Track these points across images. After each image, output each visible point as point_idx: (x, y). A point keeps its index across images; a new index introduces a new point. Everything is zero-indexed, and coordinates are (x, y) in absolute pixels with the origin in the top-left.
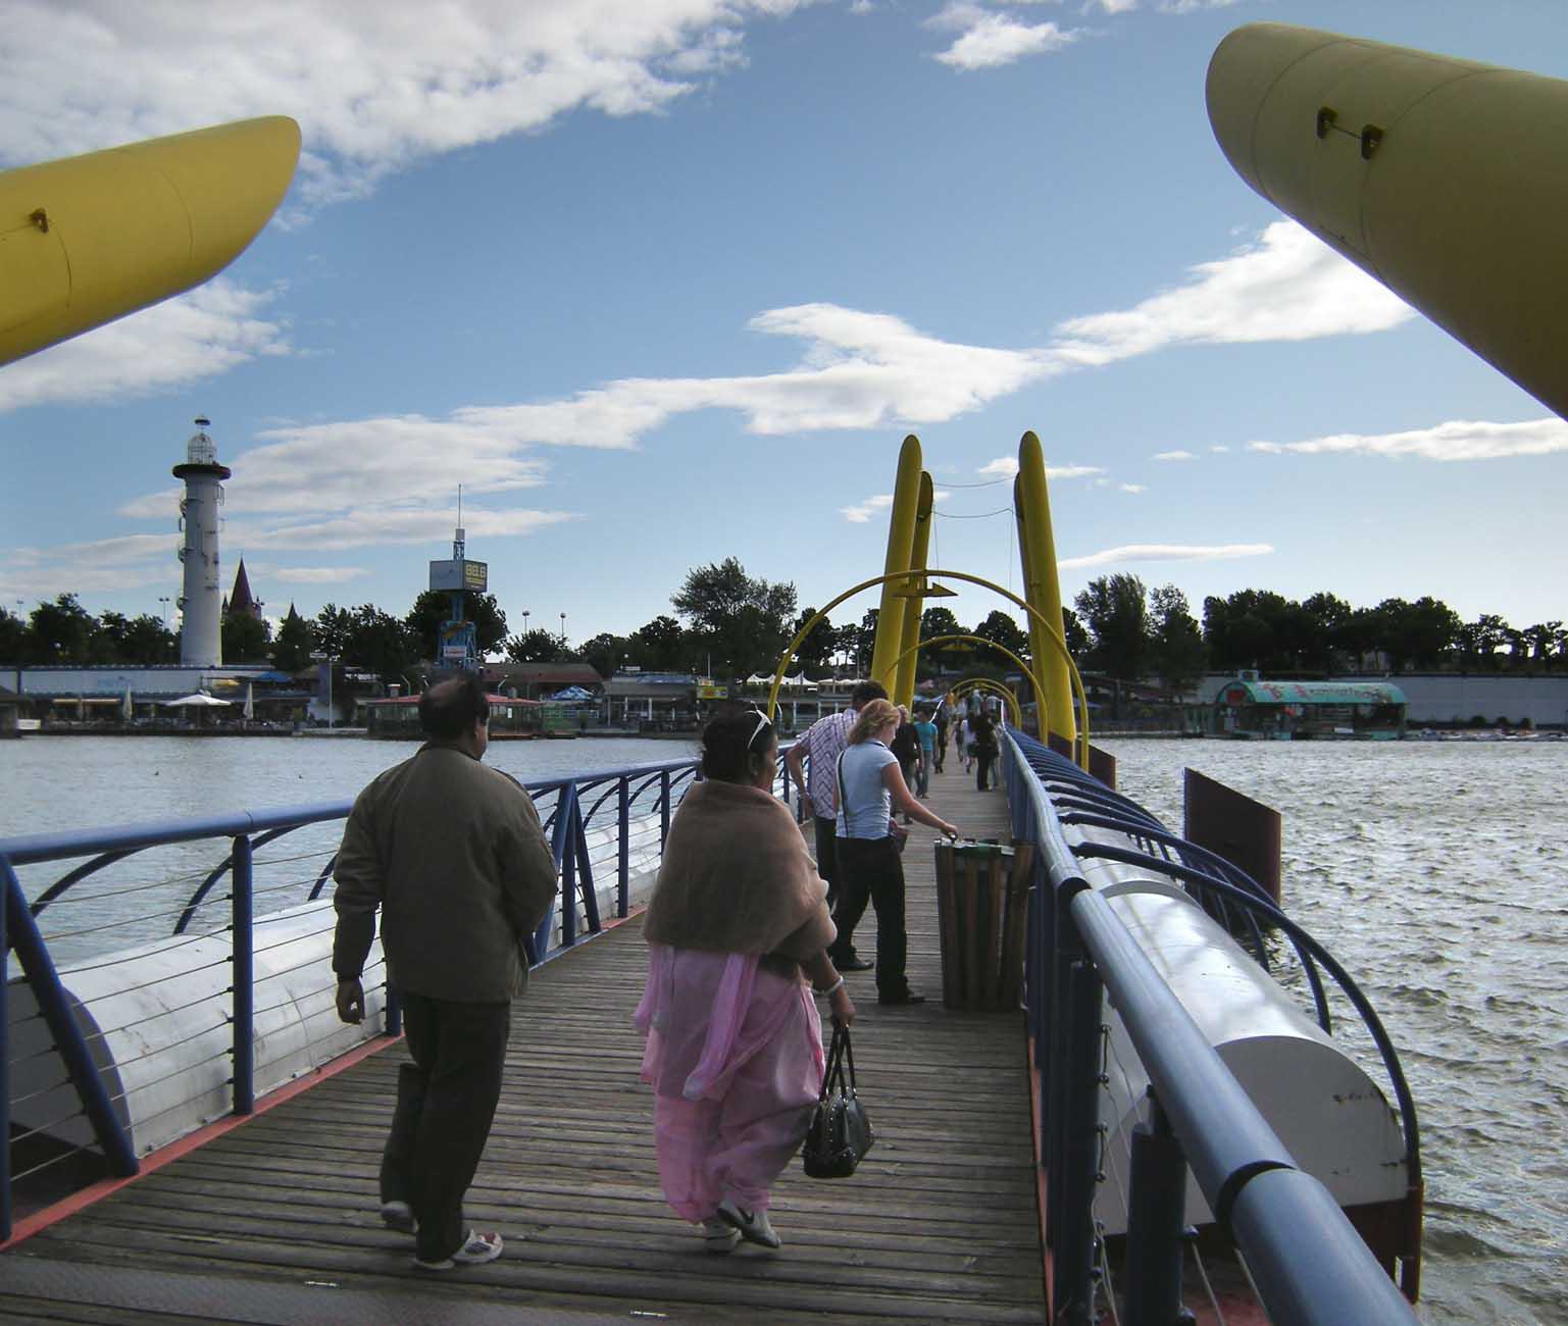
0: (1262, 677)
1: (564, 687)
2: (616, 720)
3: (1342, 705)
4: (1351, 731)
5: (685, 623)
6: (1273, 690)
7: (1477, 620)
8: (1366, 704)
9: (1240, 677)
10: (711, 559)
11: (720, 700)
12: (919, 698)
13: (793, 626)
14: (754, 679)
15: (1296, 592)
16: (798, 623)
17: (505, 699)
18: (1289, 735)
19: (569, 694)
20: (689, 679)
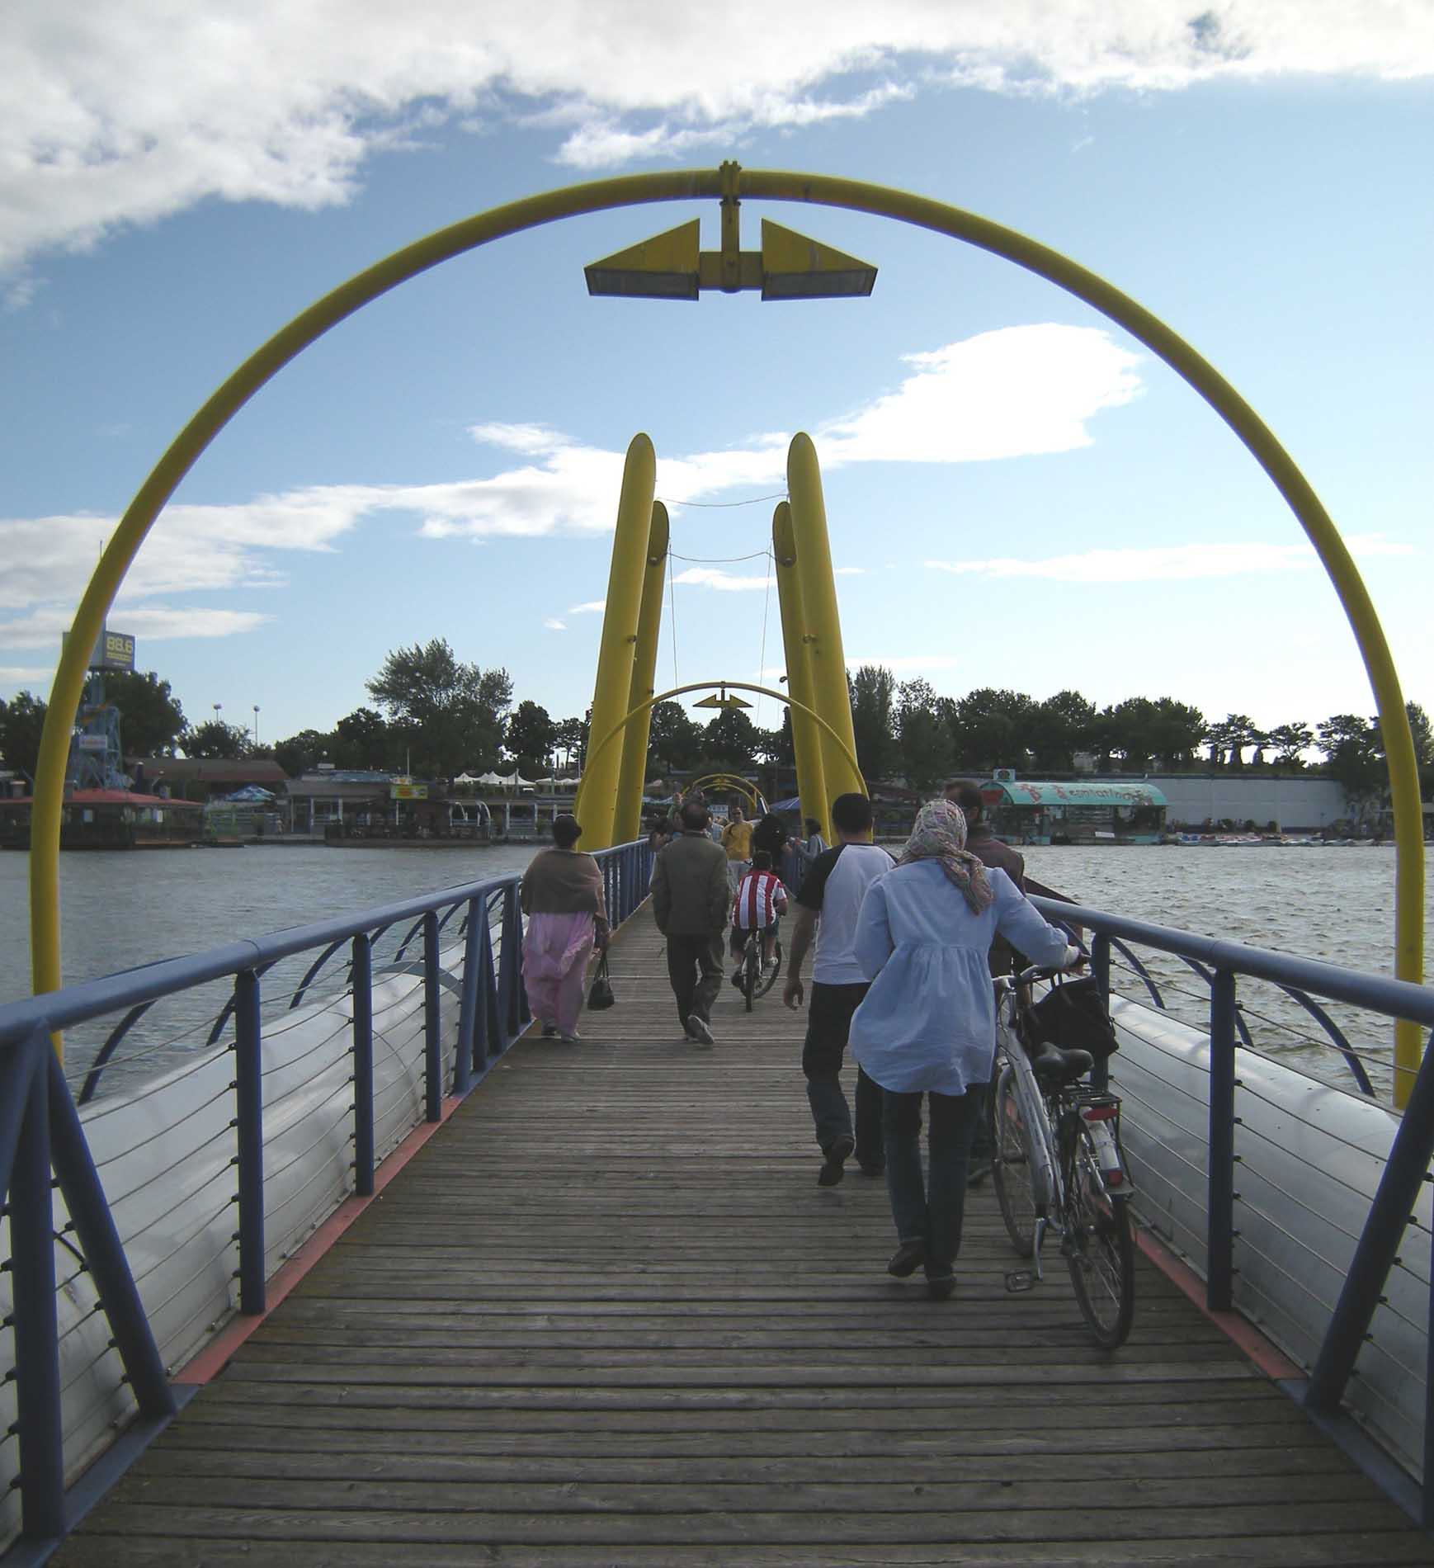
0: (1018, 778)
1: (240, 786)
2: (301, 825)
3: (1101, 807)
4: (1112, 835)
5: (385, 712)
6: (1032, 790)
7: (1225, 721)
8: (1126, 807)
9: (996, 777)
10: (415, 640)
11: (418, 801)
12: (647, 800)
13: (510, 720)
14: (465, 778)
15: (1040, 689)
16: (514, 716)
17: (156, 800)
18: (1047, 840)
19: (245, 795)
20: (377, 777)
